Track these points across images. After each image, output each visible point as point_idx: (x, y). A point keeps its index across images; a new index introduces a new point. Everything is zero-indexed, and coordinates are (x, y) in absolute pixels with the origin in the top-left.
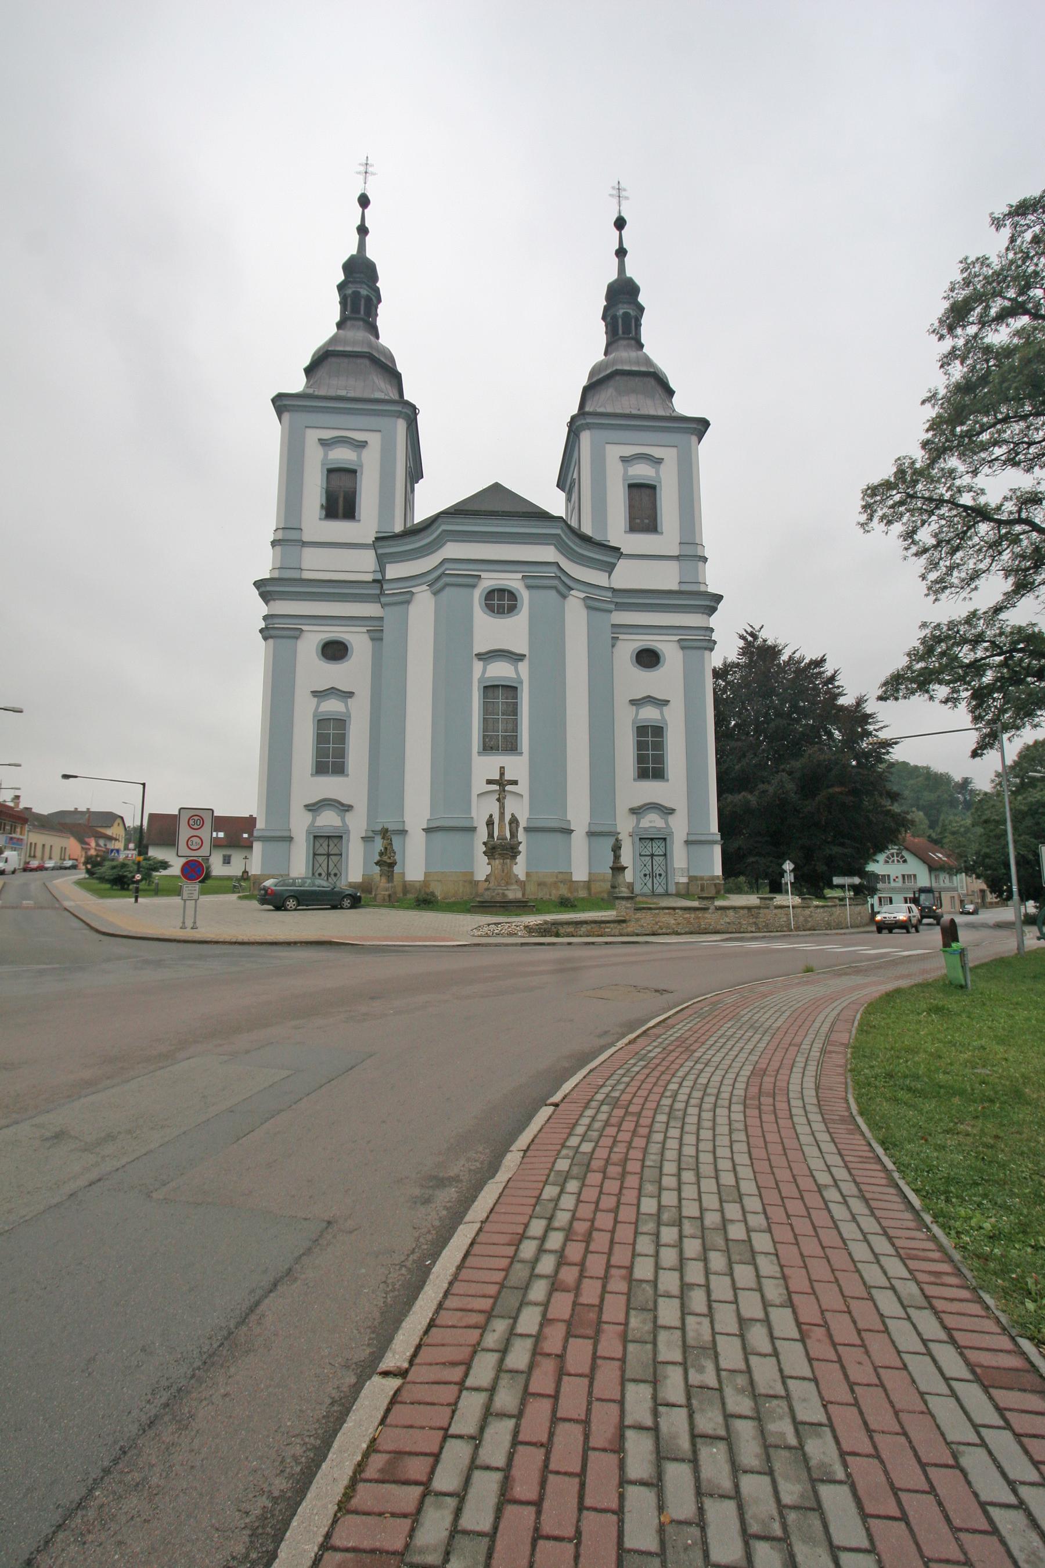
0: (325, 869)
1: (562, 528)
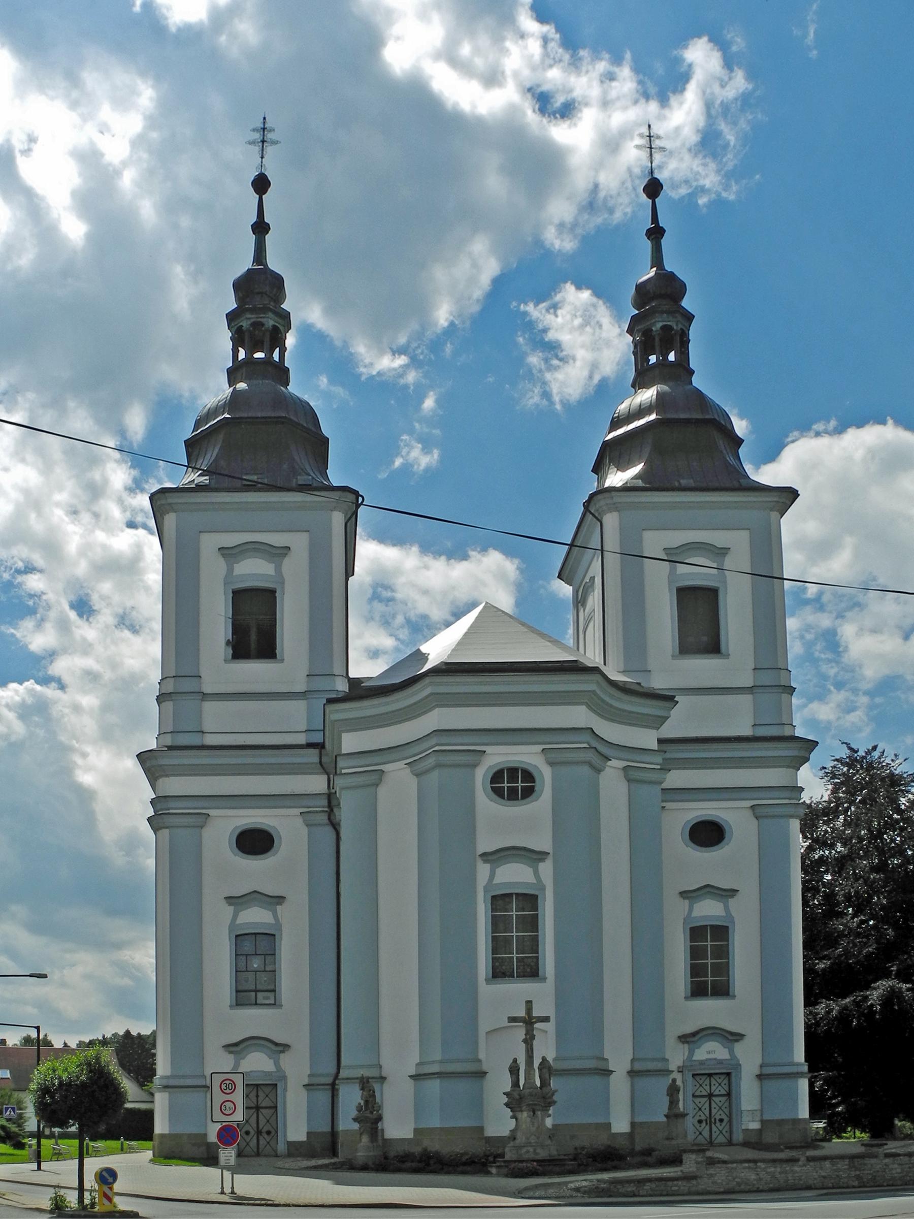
1: (598, 683)
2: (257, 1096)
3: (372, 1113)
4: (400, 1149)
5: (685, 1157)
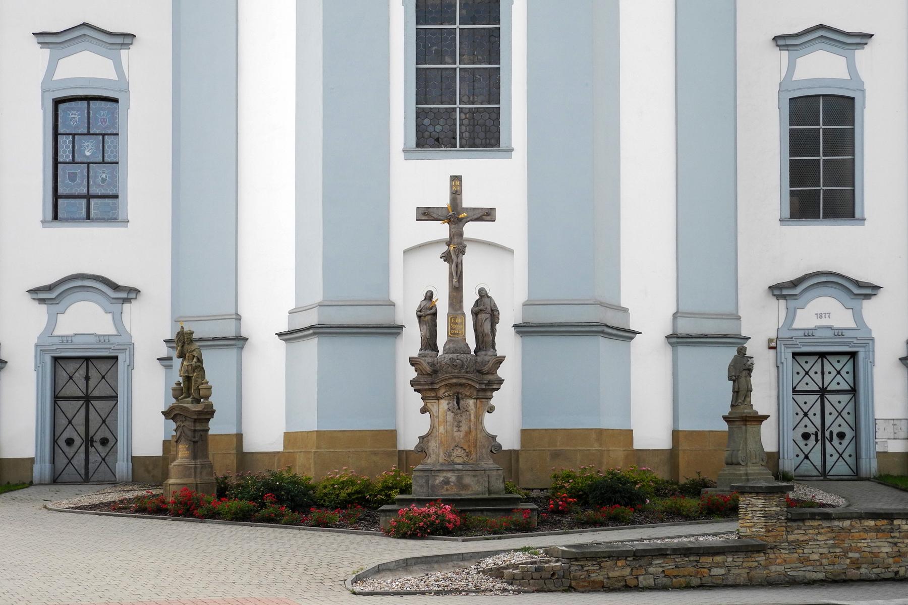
0: (82, 430)
2: (87, 378)
3: (198, 401)
4: (262, 471)
5: (743, 501)
